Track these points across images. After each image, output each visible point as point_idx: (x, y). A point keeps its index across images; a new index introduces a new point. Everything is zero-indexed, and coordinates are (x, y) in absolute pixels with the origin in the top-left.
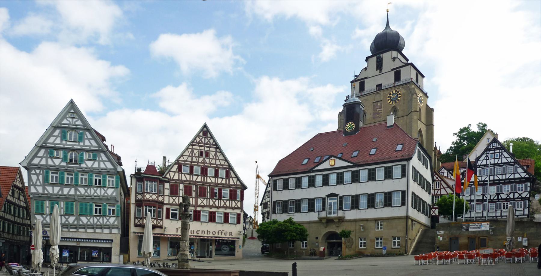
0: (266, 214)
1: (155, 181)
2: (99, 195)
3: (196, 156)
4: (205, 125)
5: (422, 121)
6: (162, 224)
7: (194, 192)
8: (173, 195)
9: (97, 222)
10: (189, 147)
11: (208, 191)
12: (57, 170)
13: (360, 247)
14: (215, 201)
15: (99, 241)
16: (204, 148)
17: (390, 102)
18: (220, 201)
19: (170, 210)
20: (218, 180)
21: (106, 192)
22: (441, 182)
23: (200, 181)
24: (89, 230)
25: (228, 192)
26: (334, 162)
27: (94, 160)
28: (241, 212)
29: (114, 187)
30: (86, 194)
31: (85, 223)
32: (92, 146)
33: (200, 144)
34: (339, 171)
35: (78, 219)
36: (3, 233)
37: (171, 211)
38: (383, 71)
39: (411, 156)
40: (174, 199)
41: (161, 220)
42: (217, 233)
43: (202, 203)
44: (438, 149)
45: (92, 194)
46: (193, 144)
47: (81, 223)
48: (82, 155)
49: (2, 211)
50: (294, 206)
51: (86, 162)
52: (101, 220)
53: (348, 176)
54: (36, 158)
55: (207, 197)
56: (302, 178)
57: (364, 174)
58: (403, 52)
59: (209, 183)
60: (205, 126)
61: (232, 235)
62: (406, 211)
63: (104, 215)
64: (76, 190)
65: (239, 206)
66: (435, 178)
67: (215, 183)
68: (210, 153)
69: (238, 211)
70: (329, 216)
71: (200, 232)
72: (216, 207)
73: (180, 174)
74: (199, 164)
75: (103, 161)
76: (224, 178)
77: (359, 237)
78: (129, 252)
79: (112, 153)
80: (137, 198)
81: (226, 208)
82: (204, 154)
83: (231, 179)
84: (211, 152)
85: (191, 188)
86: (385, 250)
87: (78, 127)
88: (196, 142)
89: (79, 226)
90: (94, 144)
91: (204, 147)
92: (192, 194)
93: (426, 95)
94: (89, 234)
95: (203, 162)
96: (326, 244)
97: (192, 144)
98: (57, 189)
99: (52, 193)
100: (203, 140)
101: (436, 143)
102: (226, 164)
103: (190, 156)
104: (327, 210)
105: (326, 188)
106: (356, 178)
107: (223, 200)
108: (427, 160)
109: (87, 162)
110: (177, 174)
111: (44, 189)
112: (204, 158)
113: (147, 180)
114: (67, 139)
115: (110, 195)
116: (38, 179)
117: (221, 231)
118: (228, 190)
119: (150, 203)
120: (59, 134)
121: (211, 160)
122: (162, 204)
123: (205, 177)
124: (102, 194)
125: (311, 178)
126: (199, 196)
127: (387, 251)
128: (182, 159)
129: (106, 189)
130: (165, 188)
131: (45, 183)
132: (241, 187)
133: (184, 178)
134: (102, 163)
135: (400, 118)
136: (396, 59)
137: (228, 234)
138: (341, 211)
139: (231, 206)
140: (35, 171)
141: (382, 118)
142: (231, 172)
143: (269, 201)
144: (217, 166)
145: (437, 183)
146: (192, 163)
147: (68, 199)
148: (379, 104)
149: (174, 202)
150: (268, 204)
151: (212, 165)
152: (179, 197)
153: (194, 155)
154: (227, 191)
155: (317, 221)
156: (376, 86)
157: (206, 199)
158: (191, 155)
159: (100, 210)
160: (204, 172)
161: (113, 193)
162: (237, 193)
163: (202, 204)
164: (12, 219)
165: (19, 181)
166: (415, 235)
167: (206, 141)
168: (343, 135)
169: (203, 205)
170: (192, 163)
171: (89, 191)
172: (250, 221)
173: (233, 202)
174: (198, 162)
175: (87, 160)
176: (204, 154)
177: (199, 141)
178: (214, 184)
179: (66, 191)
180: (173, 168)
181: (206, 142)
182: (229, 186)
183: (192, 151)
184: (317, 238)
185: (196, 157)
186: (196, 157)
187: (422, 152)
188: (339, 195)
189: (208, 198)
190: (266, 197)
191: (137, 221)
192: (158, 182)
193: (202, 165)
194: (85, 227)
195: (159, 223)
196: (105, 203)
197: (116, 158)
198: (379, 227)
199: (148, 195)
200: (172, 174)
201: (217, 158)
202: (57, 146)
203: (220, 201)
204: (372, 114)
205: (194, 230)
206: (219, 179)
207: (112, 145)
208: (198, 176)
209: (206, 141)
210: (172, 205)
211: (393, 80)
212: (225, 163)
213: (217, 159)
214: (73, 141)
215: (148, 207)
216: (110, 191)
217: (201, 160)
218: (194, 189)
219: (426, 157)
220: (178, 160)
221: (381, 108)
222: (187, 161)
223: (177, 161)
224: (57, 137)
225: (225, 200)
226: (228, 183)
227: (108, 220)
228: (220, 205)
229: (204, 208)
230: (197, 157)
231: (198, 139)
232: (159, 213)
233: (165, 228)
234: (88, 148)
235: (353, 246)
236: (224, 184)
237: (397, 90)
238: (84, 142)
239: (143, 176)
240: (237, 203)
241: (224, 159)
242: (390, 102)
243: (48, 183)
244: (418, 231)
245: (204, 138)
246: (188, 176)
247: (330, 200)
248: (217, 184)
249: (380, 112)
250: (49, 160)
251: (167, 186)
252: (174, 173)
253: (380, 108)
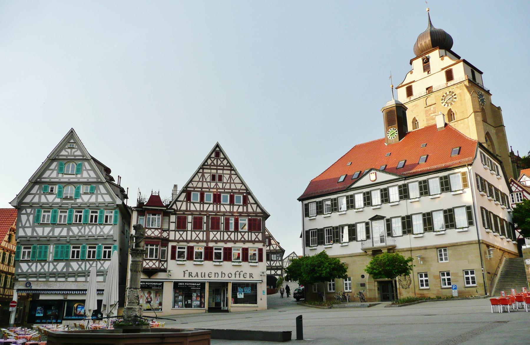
1: (159, 214)
2: (94, 235)
3: (207, 180)
4: (218, 144)
5: (488, 122)
7: (205, 225)
8: (196, 230)
10: (200, 171)
11: (222, 222)
12: (51, 207)
13: (329, 290)
14: (231, 234)
15: (82, 293)
16: (217, 171)
17: (445, 105)
18: (236, 233)
19: (176, 248)
20: (233, 207)
21: (102, 230)
22: (523, 193)
23: (212, 210)
24: (79, 279)
25: (246, 222)
27: (92, 193)
29: (112, 223)
30: (80, 234)
33: (211, 167)
35: (68, 266)
37: (178, 250)
38: (432, 71)
41: (165, 261)
42: (234, 275)
44: (516, 154)
46: (204, 167)
48: (79, 188)
50: (331, 235)
51: (82, 196)
53: (394, 193)
54: (29, 195)
55: (220, 230)
56: (339, 198)
57: (414, 189)
58: (452, 49)
59: (224, 212)
60: (218, 146)
61: (253, 278)
62: (477, 234)
63: (99, 258)
65: (261, 239)
66: (513, 189)
67: (230, 212)
68: (223, 176)
71: (213, 275)
72: (231, 241)
74: (211, 190)
75: (102, 194)
77: (418, 273)
79: (118, 186)
81: (244, 242)
82: (217, 178)
83: (249, 205)
84: (224, 175)
85: (201, 219)
86: (456, 290)
87: (77, 157)
88: (208, 165)
89: (69, 274)
90: (93, 175)
91: (217, 169)
92: (203, 227)
93: (488, 92)
94: (79, 284)
95: (215, 187)
96: (376, 283)
97: (203, 167)
98: (47, 230)
99: (42, 235)
100: (215, 162)
101: (511, 147)
102: (243, 187)
103: (201, 182)
105: (368, 209)
106: (404, 194)
107: (240, 232)
108: (496, 166)
109: (83, 196)
110: (185, 203)
111: (34, 230)
112: (217, 183)
113: (149, 213)
114: (64, 172)
115: (106, 233)
116: (28, 219)
117: (238, 273)
118: (247, 219)
119: (151, 240)
120: (55, 167)
121: (224, 184)
122: (165, 242)
123: (218, 206)
126: (212, 228)
127: (459, 293)
128: (190, 185)
129: (103, 226)
130: (171, 221)
131: (35, 224)
132: (262, 215)
133: (192, 208)
134: (100, 196)
135: (459, 122)
137: (248, 276)
138: (390, 238)
139: (250, 239)
140: (26, 211)
145: (517, 194)
146: (203, 190)
147: (58, 241)
148: (432, 109)
149: (181, 237)
151: (226, 191)
152: (187, 231)
153: (204, 180)
154: (245, 220)
155: (361, 253)
157: (219, 233)
158: (201, 180)
159: (94, 252)
160: (217, 199)
162: (230, 222)
166: (497, 266)
167: (219, 162)
169: (216, 239)
170: (203, 190)
171: (83, 231)
172: (294, 258)
173: (253, 234)
175: (83, 194)
176: (217, 178)
177: (211, 163)
178: (230, 213)
179: (57, 231)
180: (180, 197)
181: (218, 164)
182: (248, 214)
183: (203, 176)
185: (207, 182)
186: (207, 182)
187: (486, 155)
189: (222, 230)
192: (162, 214)
193: (215, 192)
194: (75, 274)
195: (163, 265)
196: (100, 244)
197: (119, 190)
198: (443, 257)
199: (150, 231)
201: (232, 181)
202: (52, 180)
203: (236, 233)
204: (425, 120)
205: (205, 273)
207: (119, 176)
208: (210, 204)
209: (219, 162)
210: (178, 241)
212: (241, 186)
213: (232, 183)
214: (70, 173)
215: (149, 245)
216: (107, 230)
217: (213, 185)
218: (205, 221)
219: (493, 161)
220: (187, 187)
222: (196, 187)
223: (185, 188)
224: (53, 170)
225: (243, 232)
226: (245, 210)
227: (102, 265)
228: (236, 239)
229: (217, 243)
230: (208, 182)
231: (209, 162)
232: (163, 252)
233: (169, 271)
234: (86, 180)
235: (412, 286)
237: (451, 90)
238: (82, 174)
240: (216, 234)
242: (445, 105)
243: (38, 223)
244: (501, 260)
245: (216, 160)
246: (197, 206)
248: (232, 213)
250: (43, 196)
251: (173, 218)
252: (181, 203)
253: (433, 113)
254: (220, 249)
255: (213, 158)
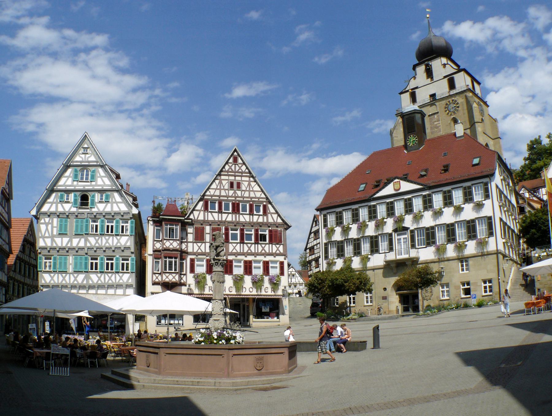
0: (313, 262)
2: (111, 246)
6: (185, 281)
9: (109, 281)
26: (399, 185)
28: (285, 259)
31: (95, 282)
32: (105, 185)
34: (406, 197)
36: (13, 297)
38: (435, 79)
39: (492, 171)
40: (199, 246)
43: (234, 250)
45: (103, 245)
47: (90, 282)
49: (13, 271)
50: (423, 236)
52: (113, 278)
64: (86, 240)
65: (282, 252)
68: (242, 183)
69: (281, 259)
70: (399, 257)
73: (206, 213)
74: (229, 198)
75: (117, 203)
76: (261, 215)
78: (146, 319)
80: (155, 248)
83: (269, 215)
84: (243, 182)
88: (225, 171)
91: (235, 176)
100: (233, 167)
102: (263, 196)
103: (218, 189)
104: (396, 250)
110: (202, 213)
116: (47, 229)
123: (238, 215)
124: (114, 245)
125: (371, 208)
133: (210, 218)
136: (447, 65)
140: (45, 220)
141: (442, 133)
142: (270, 206)
143: (319, 243)
144: (251, 199)
146: (221, 198)
150: (315, 249)
153: (222, 188)
156: (429, 97)
161: (127, 242)
163: (234, 251)
164: (22, 281)
165: (30, 235)
167: (237, 168)
168: (405, 151)
170: (221, 198)
171: (100, 241)
174: (227, 196)
177: (229, 169)
183: (221, 183)
184: (385, 289)
185: (225, 190)
186: (225, 190)
188: (409, 228)
190: (312, 239)
191: (154, 278)
193: (233, 200)
196: (118, 256)
200: (196, 213)
201: (251, 189)
206: (254, 216)
211: (447, 89)
212: (261, 195)
217: (231, 192)
221: (439, 121)
226: (265, 221)
227: (121, 278)
228: (256, 252)
236: (261, 223)
239: (162, 218)
241: (260, 190)
247: (398, 235)
248: (220, 223)
249: (438, 125)
250: (59, 205)
254: (203, 261)
255: (231, 163)
